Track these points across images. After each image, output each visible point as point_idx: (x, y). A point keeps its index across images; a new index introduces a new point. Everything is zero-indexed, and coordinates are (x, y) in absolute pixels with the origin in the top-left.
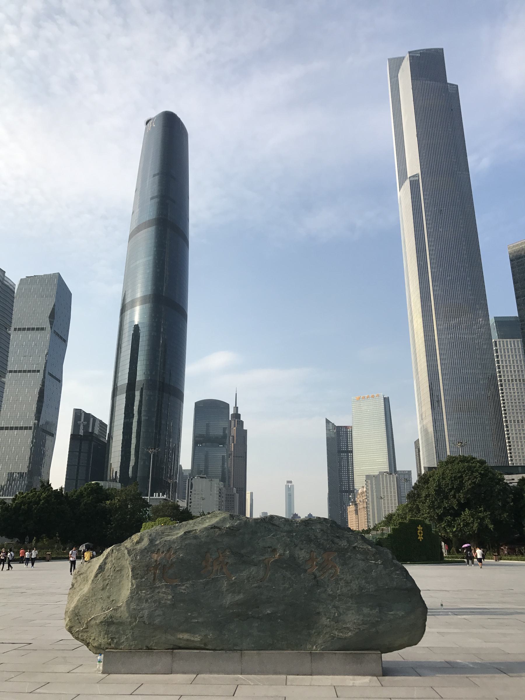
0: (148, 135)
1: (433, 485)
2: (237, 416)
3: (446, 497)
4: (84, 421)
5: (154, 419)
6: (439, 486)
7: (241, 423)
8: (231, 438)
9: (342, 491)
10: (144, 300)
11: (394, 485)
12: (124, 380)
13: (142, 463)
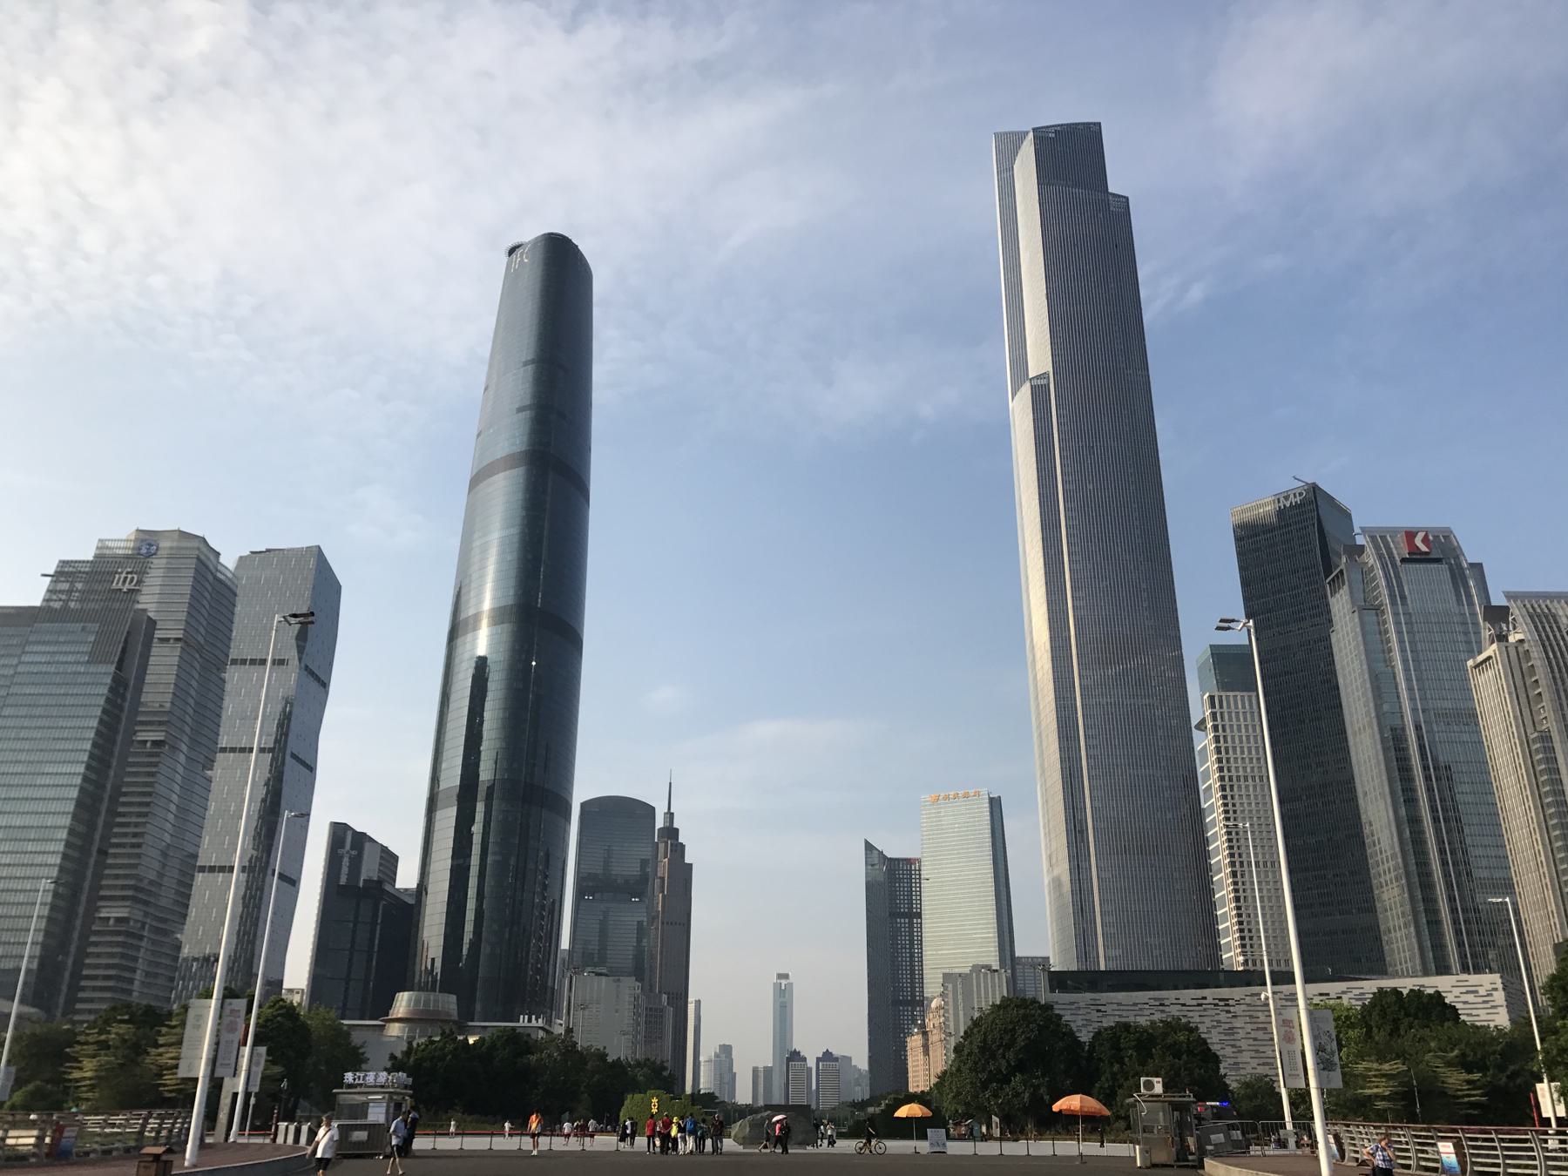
0: (511, 278)
1: (978, 1039)
2: (671, 832)
3: (993, 1056)
4: (352, 848)
6: (985, 1041)
7: (679, 849)
8: (657, 881)
10: (499, 616)
13: (488, 950)
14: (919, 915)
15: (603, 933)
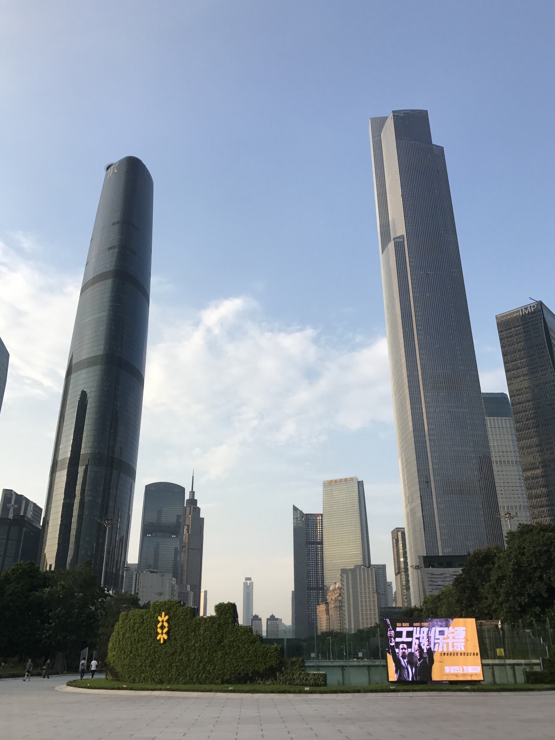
2: (193, 502)
4: (15, 504)
5: (99, 500)
6: (518, 563)
8: (186, 527)
9: (310, 589)
11: (373, 581)
12: (66, 453)
14: (321, 543)
15: (156, 554)
